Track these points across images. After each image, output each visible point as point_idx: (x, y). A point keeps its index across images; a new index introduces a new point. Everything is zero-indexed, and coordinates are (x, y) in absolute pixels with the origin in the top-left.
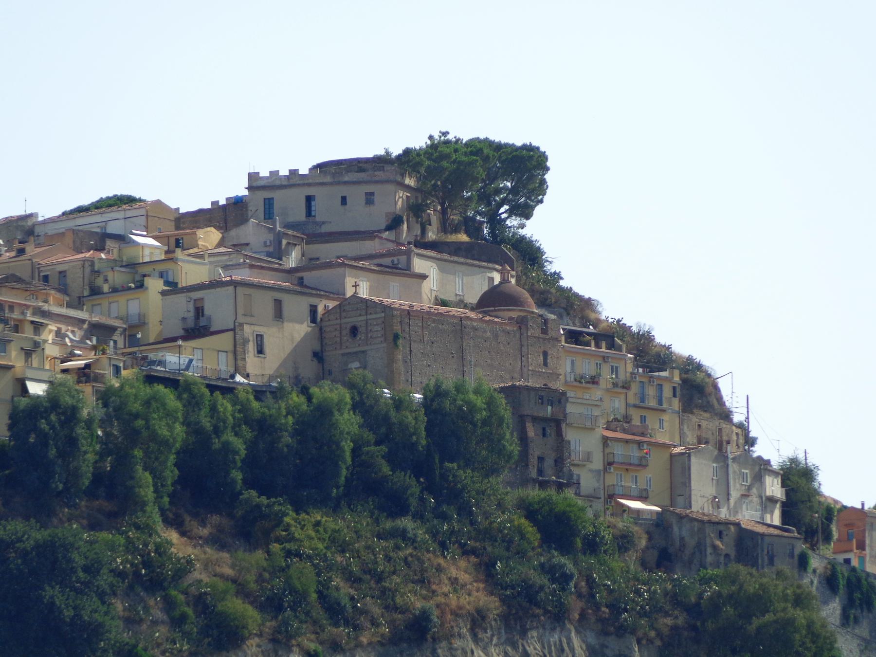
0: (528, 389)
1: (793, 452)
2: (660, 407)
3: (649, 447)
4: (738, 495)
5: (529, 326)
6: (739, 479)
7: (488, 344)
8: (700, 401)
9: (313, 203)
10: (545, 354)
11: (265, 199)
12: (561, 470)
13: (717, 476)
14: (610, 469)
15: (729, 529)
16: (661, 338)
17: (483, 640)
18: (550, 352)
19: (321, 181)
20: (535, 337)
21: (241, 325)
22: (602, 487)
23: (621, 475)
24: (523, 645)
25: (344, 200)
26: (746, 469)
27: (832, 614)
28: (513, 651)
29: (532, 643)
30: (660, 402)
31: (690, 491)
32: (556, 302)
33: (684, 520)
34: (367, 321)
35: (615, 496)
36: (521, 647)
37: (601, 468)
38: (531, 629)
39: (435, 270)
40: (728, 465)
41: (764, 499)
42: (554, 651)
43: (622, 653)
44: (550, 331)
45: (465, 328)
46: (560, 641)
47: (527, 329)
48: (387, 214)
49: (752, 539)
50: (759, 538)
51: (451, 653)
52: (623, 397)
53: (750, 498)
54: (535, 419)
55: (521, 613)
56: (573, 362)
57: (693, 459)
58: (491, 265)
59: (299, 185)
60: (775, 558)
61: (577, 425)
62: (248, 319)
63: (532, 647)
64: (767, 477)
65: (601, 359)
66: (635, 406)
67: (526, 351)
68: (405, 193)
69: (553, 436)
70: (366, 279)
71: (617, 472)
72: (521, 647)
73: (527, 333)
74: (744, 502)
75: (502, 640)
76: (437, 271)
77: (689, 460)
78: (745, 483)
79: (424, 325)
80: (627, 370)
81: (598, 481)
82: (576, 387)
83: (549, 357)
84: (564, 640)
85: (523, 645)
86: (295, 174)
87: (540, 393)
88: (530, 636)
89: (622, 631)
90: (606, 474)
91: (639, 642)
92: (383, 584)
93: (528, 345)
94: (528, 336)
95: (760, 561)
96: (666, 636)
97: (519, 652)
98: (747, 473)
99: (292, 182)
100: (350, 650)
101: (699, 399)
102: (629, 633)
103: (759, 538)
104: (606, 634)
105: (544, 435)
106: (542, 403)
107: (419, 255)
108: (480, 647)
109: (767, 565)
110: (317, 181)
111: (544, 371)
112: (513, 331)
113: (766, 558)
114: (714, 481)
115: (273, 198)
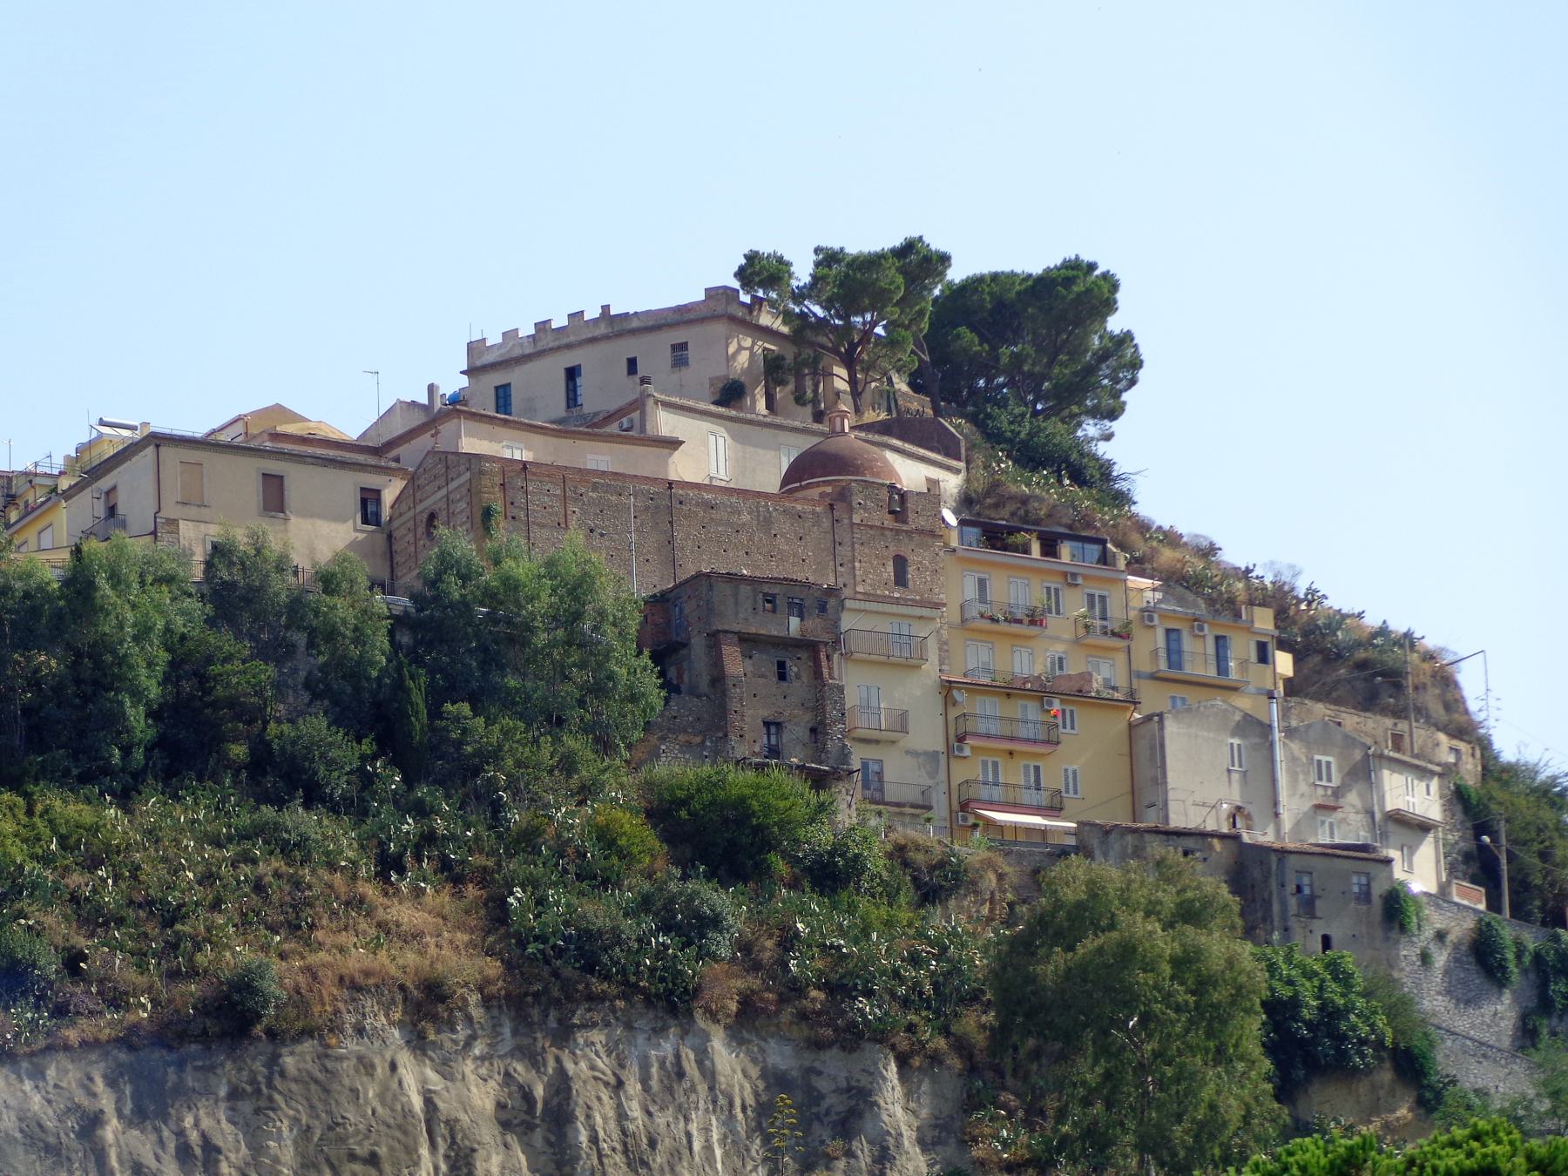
0: (733, 579)
1: (1516, 751)
2: (1222, 681)
3: (1068, 708)
4: (1306, 806)
5: (854, 504)
6: (1307, 773)
7: (743, 537)
8: (1392, 700)
9: (579, 381)
10: (900, 563)
11: (497, 388)
12: (823, 750)
13: (1240, 766)
14: (961, 749)
15: (1211, 847)
16: (1234, 555)
17: (441, 1047)
18: (911, 558)
19: (590, 335)
20: (871, 527)
21: (173, 523)
22: (944, 787)
23: (995, 764)
24: (558, 1060)
25: (632, 365)
26: (1327, 755)
27: (1488, 1026)
28: (528, 1070)
29: (585, 1056)
30: (1222, 669)
31: (1166, 792)
32: (1049, 516)
33: (1112, 837)
34: (447, 496)
35: (972, 805)
36: (551, 1064)
37: (940, 746)
38: (587, 1026)
39: (721, 441)
40: (1272, 745)
41: (1378, 816)
42: (655, 1077)
43: (854, 1084)
44: (911, 516)
45: (681, 503)
46: (678, 1056)
47: (851, 510)
48: (712, 381)
49: (1262, 863)
50: (1274, 858)
51: (324, 1066)
52: (1121, 658)
53: (1339, 815)
54: (749, 642)
55: (556, 993)
56: (982, 584)
57: (1171, 728)
58: (886, 439)
59: (552, 350)
60: (1318, 903)
61: (865, 656)
62: (193, 511)
63: (583, 1065)
64: (1386, 773)
65: (1061, 579)
66: (1154, 677)
67: (849, 554)
68: (760, 343)
69: (805, 679)
70: (522, 446)
71: (985, 758)
72: (551, 1064)
73: (851, 518)
74: (1323, 823)
75: (504, 1049)
76: (729, 440)
77: (1162, 728)
78: (1324, 783)
79: (569, 493)
80: (1131, 604)
81: (933, 774)
82: (981, 631)
83: (910, 569)
84: (689, 1057)
85: (558, 1060)
86: (545, 330)
87: (766, 589)
88: (581, 1041)
89: (853, 1037)
90: (953, 763)
91: (903, 1062)
92: (178, 927)
93: (853, 544)
94: (852, 525)
95: (1276, 908)
96: (981, 1051)
97: (545, 1074)
98: (1328, 764)
99: (541, 346)
100: (33, 1054)
101: (1391, 697)
102: (869, 1039)
103: (1274, 858)
104: (818, 1045)
105: (782, 676)
106: (774, 611)
107: (667, 405)
108: (432, 1059)
109: (1298, 915)
110: (584, 337)
111: (896, 595)
112: (813, 513)
113: (1293, 902)
114: (1235, 777)
115: (509, 385)
